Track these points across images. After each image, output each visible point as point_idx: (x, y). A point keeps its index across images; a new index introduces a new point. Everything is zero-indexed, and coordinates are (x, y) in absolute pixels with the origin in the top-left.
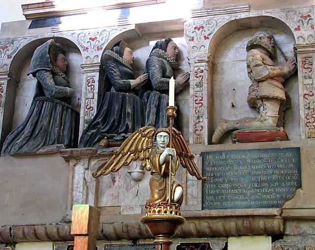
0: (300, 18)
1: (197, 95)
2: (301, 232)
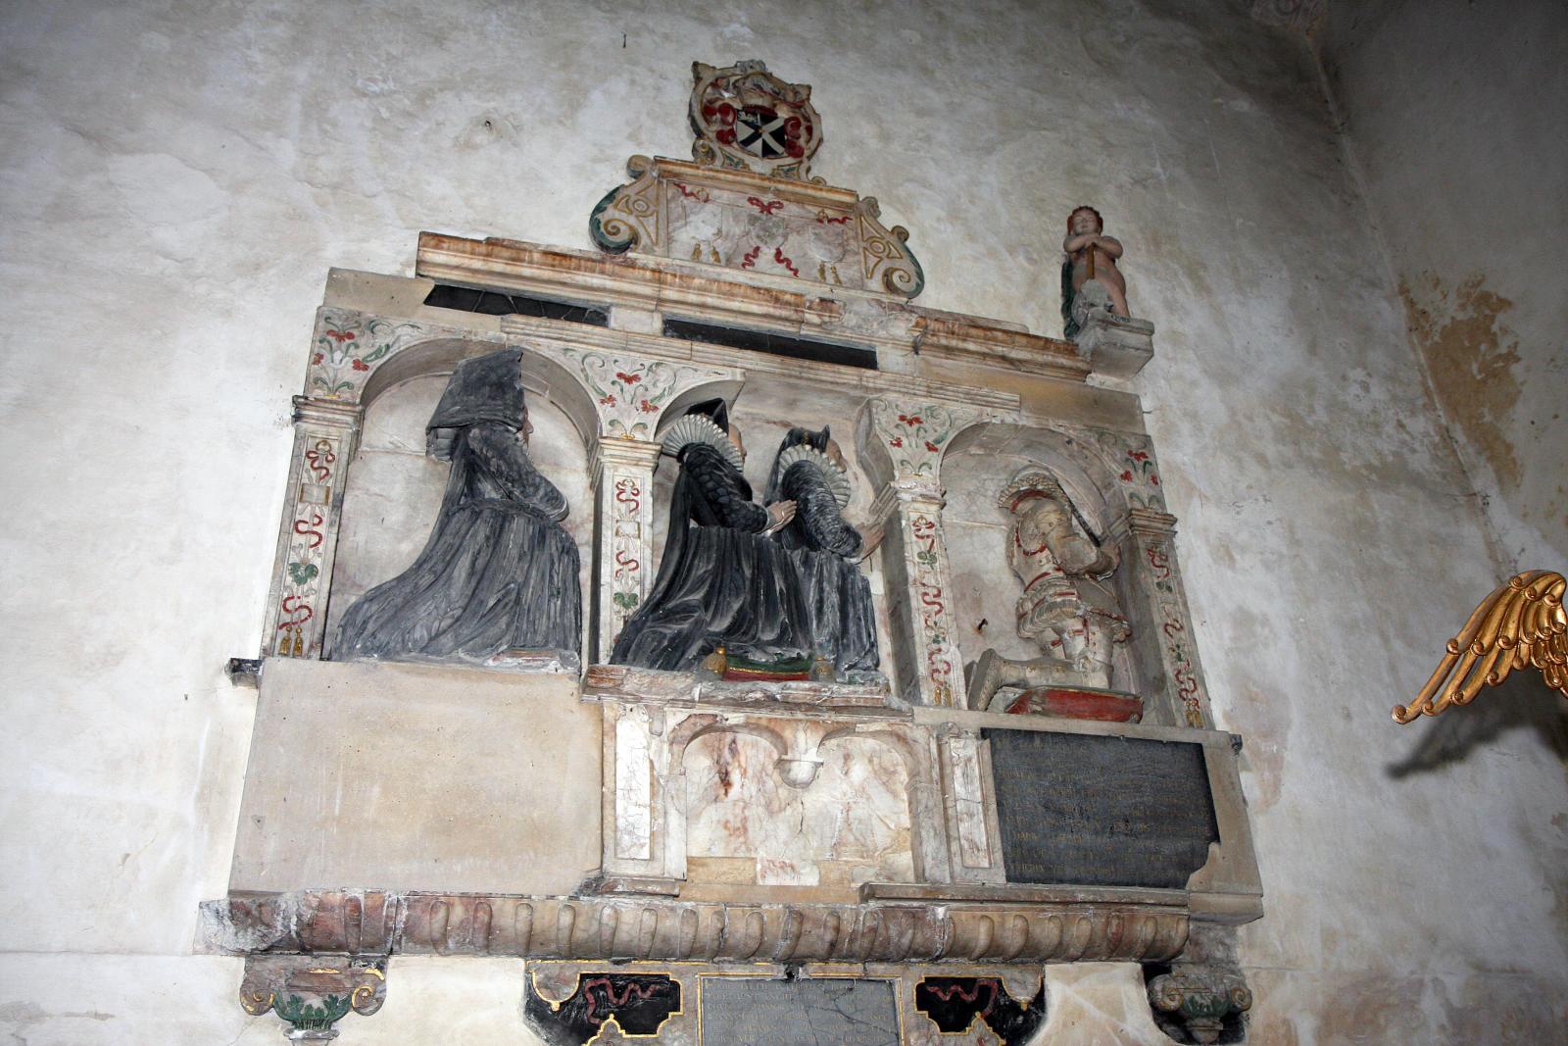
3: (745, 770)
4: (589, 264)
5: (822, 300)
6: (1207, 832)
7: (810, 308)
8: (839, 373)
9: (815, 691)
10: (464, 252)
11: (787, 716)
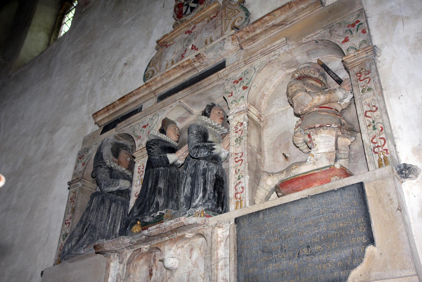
0: (347, 28)
1: (236, 152)
2: (233, 31)
3: (157, 267)
4: (130, 95)
5: (196, 56)
6: (364, 239)
7: (194, 62)
8: (210, 79)
9: (158, 228)
10: (103, 113)
11: (160, 241)
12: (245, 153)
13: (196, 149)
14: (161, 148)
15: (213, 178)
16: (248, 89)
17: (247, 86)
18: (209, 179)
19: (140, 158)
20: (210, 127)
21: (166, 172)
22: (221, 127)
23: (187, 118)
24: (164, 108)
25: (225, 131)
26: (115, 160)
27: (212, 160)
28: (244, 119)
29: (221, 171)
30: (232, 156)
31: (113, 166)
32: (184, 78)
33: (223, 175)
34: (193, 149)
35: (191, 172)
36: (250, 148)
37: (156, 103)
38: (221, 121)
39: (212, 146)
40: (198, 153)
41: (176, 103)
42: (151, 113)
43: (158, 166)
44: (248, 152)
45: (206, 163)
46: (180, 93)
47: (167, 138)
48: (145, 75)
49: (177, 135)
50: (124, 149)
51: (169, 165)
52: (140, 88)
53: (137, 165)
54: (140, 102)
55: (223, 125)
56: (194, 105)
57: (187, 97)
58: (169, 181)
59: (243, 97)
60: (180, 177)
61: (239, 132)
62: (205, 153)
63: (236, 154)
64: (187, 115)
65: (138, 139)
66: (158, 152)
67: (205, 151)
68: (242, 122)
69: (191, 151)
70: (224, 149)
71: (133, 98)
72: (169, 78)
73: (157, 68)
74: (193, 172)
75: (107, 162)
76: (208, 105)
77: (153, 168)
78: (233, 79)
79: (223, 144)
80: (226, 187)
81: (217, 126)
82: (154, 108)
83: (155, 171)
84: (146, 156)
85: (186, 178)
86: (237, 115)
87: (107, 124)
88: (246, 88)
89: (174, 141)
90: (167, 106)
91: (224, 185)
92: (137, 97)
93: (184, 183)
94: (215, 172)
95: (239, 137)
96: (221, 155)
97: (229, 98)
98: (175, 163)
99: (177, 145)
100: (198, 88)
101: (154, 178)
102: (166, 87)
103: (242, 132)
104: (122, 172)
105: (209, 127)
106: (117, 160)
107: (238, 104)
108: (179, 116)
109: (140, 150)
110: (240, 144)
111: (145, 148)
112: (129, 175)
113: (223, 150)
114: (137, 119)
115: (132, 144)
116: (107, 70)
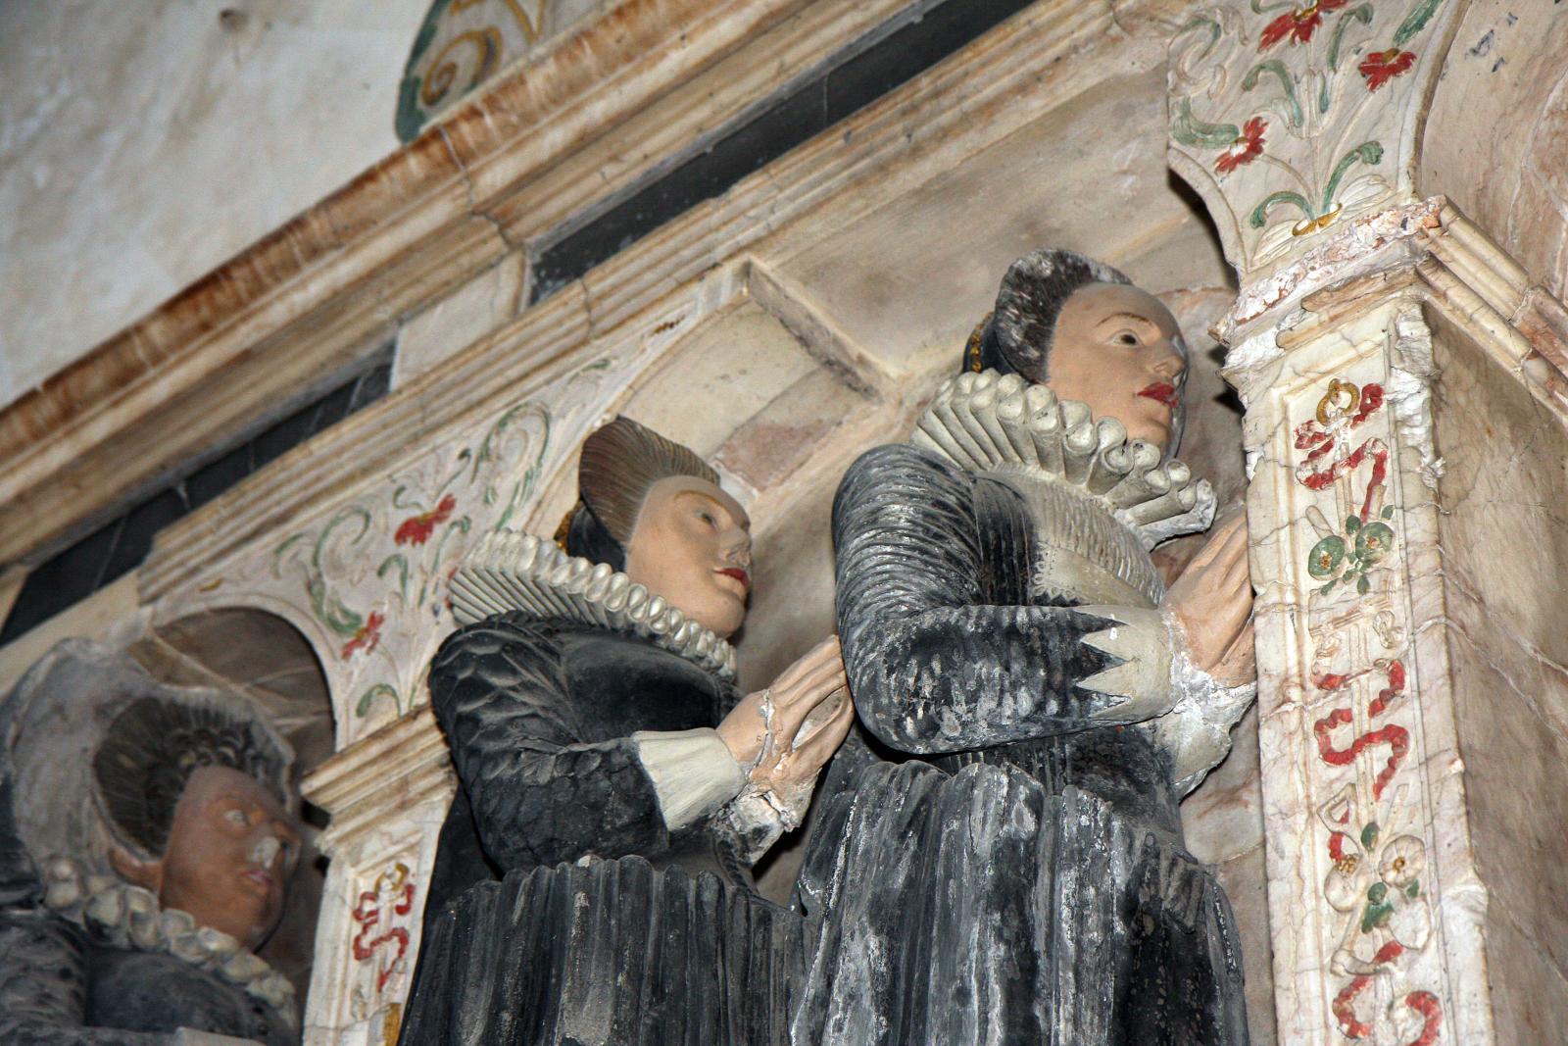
1: (1335, 666)
4: (274, 254)
12: (1429, 664)
13: (924, 664)
14: (579, 690)
15: (1108, 927)
16: (1419, 74)
17: (1404, 48)
18: (1067, 936)
19: (372, 814)
20: (1047, 477)
21: (628, 903)
22: (1159, 466)
23: (812, 433)
24: (599, 349)
25: (1196, 501)
26: (138, 859)
27: (1076, 769)
28: (1396, 348)
29: (1179, 870)
30: (1286, 700)
31: (108, 911)
32: (778, 54)
33: (1201, 907)
34: (895, 661)
35: (884, 879)
36: (1472, 616)
37: (523, 307)
38: (1151, 420)
39: (1075, 629)
40: (944, 696)
41: (714, 293)
42: (481, 402)
43: (550, 851)
44: (1456, 650)
45: (1023, 792)
46: (747, 191)
47: (636, 598)
48: (409, 88)
49: (727, 572)
50: (225, 761)
51: (663, 844)
52: (369, 176)
53: (344, 884)
54: (371, 310)
55: (1172, 449)
56: (882, 301)
57: (816, 228)
58: (658, 989)
59: (1370, 152)
60: (767, 942)
61: (1344, 472)
62: (1008, 700)
63: (1329, 683)
64: (814, 402)
65: (358, 642)
66: (547, 721)
67: (1015, 686)
68: (1376, 379)
69: (874, 680)
70: (1196, 660)
71: (303, 285)
72: (638, 71)
73: (525, 7)
74: (900, 880)
75: (55, 879)
76: (1019, 273)
77: (499, 875)
78: (1256, 9)
79: (1186, 620)
80: (1238, 1028)
81: (1118, 460)
82: (503, 355)
83: (521, 902)
84: (434, 788)
85: (836, 943)
86: (1312, 319)
87: (64, 545)
88: (1394, 70)
89: (704, 628)
90: (621, 324)
91: (1218, 1010)
92: (346, 269)
93: (809, 992)
94: (1119, 875)
95: (1352, 524)
96: (1166, 724)
97: (1230, 180)
98: (720, 828)
99: (728, 668)
100: (925, 130)
101: (515, 957)
102: (614, 158)
103: (1379, 470)
104: (196, 966)
105: (1033, 470)
106: (153, 863)
107: (1321, 222)
108: (742, 418)
109: (375, 736)
110: (1364, 587)
111: (428, 719)
112: (265, 1002)
113: (1188, 672)
114: (349, 468)
115: (299, 722)
116: (64, 90)
